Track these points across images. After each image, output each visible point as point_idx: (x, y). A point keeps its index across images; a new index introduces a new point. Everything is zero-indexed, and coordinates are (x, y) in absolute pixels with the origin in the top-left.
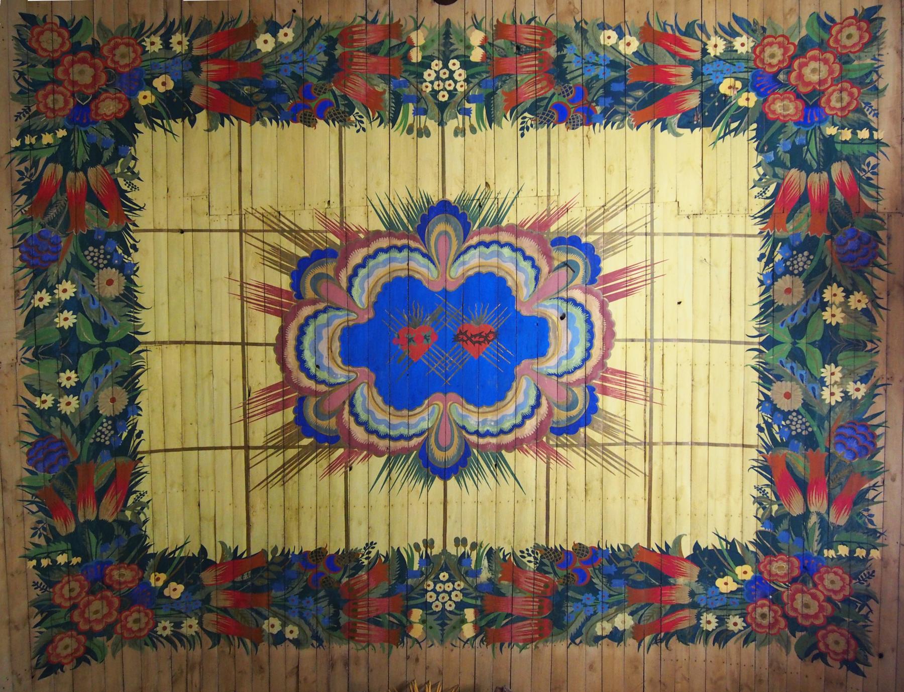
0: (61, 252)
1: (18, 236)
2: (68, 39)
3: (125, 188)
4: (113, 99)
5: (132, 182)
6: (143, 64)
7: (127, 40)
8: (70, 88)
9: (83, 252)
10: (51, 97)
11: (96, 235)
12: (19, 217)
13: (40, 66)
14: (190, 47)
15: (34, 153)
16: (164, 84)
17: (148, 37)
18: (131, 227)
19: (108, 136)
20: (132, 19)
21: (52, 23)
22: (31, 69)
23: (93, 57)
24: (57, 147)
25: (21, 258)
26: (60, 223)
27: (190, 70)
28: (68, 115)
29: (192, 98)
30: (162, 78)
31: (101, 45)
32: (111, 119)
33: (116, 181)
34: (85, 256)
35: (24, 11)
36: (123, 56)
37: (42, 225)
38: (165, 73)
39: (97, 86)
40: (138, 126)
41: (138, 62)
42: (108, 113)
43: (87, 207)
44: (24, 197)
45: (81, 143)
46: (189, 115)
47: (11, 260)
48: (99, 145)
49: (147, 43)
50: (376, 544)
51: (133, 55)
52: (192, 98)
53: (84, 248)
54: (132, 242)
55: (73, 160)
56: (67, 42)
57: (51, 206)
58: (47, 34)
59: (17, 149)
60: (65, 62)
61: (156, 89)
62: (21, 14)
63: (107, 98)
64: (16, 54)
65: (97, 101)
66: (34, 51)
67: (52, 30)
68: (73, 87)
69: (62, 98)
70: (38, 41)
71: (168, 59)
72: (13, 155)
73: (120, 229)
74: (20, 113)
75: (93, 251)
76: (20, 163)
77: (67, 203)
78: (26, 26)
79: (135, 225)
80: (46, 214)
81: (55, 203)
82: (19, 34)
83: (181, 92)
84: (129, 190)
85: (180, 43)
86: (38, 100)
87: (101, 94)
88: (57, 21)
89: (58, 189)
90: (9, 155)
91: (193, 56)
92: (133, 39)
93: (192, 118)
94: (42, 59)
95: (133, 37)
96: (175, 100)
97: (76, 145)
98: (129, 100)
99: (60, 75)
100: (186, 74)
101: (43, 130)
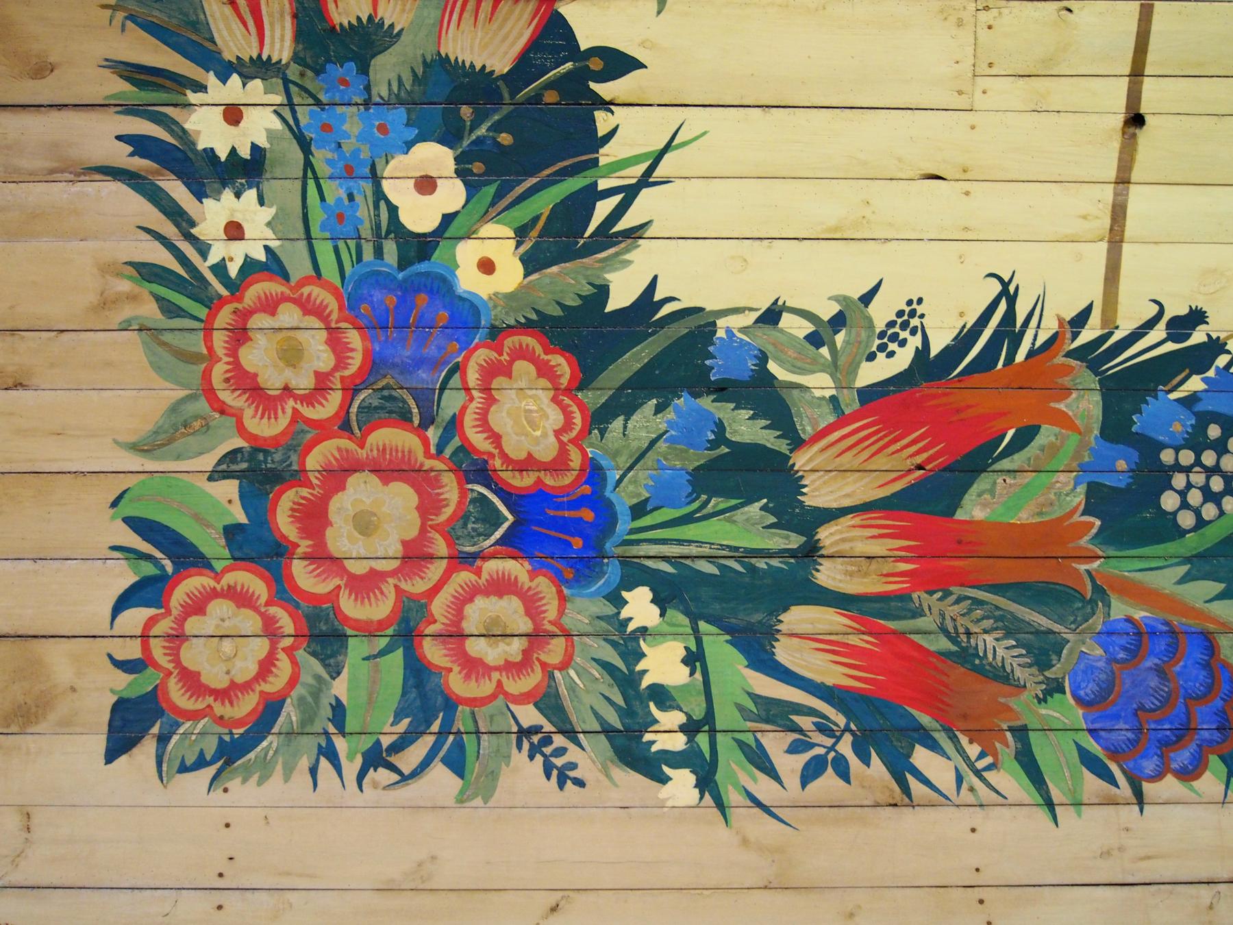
0: (1175, 620)
1: (1092, 784)
2: (217, 577)
3: (903, 358)
4: (490, 400)
5: (880, 326)
6: (330, 271)
7: (220, 340)
8: (436, 571)
9: (1182, 533)
10: (476, 647)
11: (1108, 480)
12: (1009, 780)
13: (340, 688)
14: (258, 68)
15: (726, 717)
16: (426, 185)
17: (204, 251)
18: (1088, 335)
19: (661, 422)
20: (117, 317)
21: (145, 637)
22: (351, 724)
23: (299, 477)
24: (703, 626)
25: (1188, 774)
26: (1043, 622)
27: (364, 70)
28: (559, 580)
29: (501, 63)
30: (399, 192)
31: (239, 443)
32: (582, 406)
33: (869, 394)
34: (1201, 523)
35: (99, 743)
36: (291, 355)
37: (1049, 693)
38: (376, 179)
39: (428, 464)
40: (622, 295)
41: (318, 294)
42: (555, 418)
43: (979, 514)
44: (921, 757)
45: (689, 532)
46: (580, 78)
47: (1199, 811)
48: (699, 457)
49: (235, 255)
50: (920, 301)
51: (289, 315)
52: (501, 63)
53: (1167, 529)
54: (1159, 333)
55: (761, 564)
56: (230, 579)
57: (966, 656)
58: (195, 656)
59: (706, 783)
60: (323, 588)
61: (448, 219)
62: (111, 756)
63: (484, 422)
64: (287, 778)
65: (498, 463)
66: (271, 708)
67: (177, 638)
68: (431, 558)
69: (480, 602)
70: (226, 694)
71: (308, 164)
72: (733, 797)
73: (1092, 381)
74: (548, 770)
75: (1183, 494)
76: (776, 777)
77: (955, 589)
78: (163, 739)
79: (1081, 319)
80: (1002, 676)
81: (954, 640)
82: (201, 763)
83: (466, 111)
84: (915, 342)
85: (233, 114)
86: (493, 697)
87: (466, 448)
88: (135, 617)
89: (892, 625)
90: (733, 814)
91: (296, 58)
92: (212, 316)
93: (596, 64)
94: (306, 678)
95: (203, 312)
96: (505, 139)
97: (693, 550)
98: (496, 333)
99: (380, 608)
100: (381, 90)
101: (627, 681)
